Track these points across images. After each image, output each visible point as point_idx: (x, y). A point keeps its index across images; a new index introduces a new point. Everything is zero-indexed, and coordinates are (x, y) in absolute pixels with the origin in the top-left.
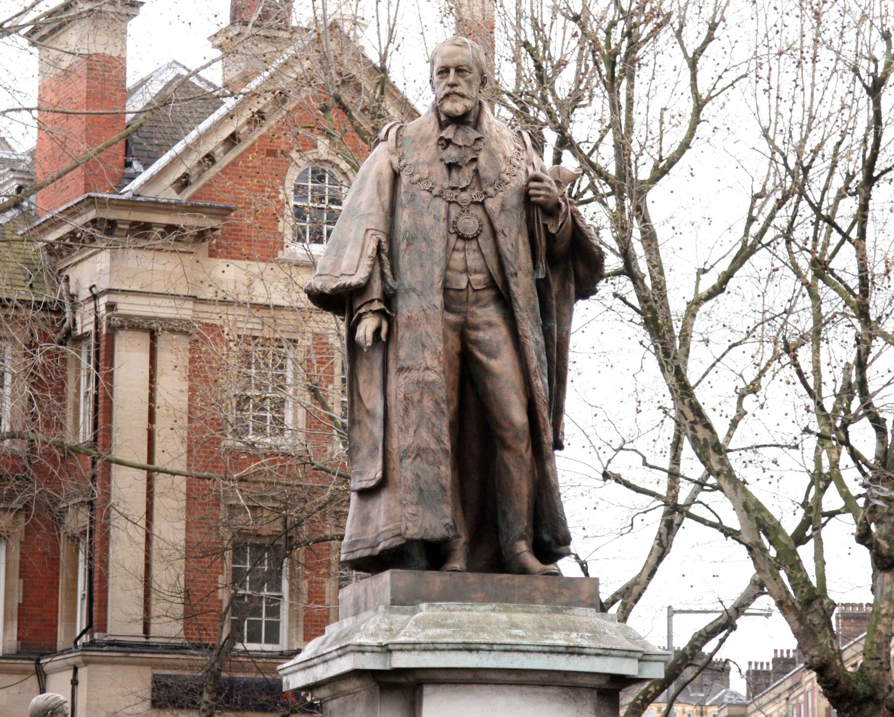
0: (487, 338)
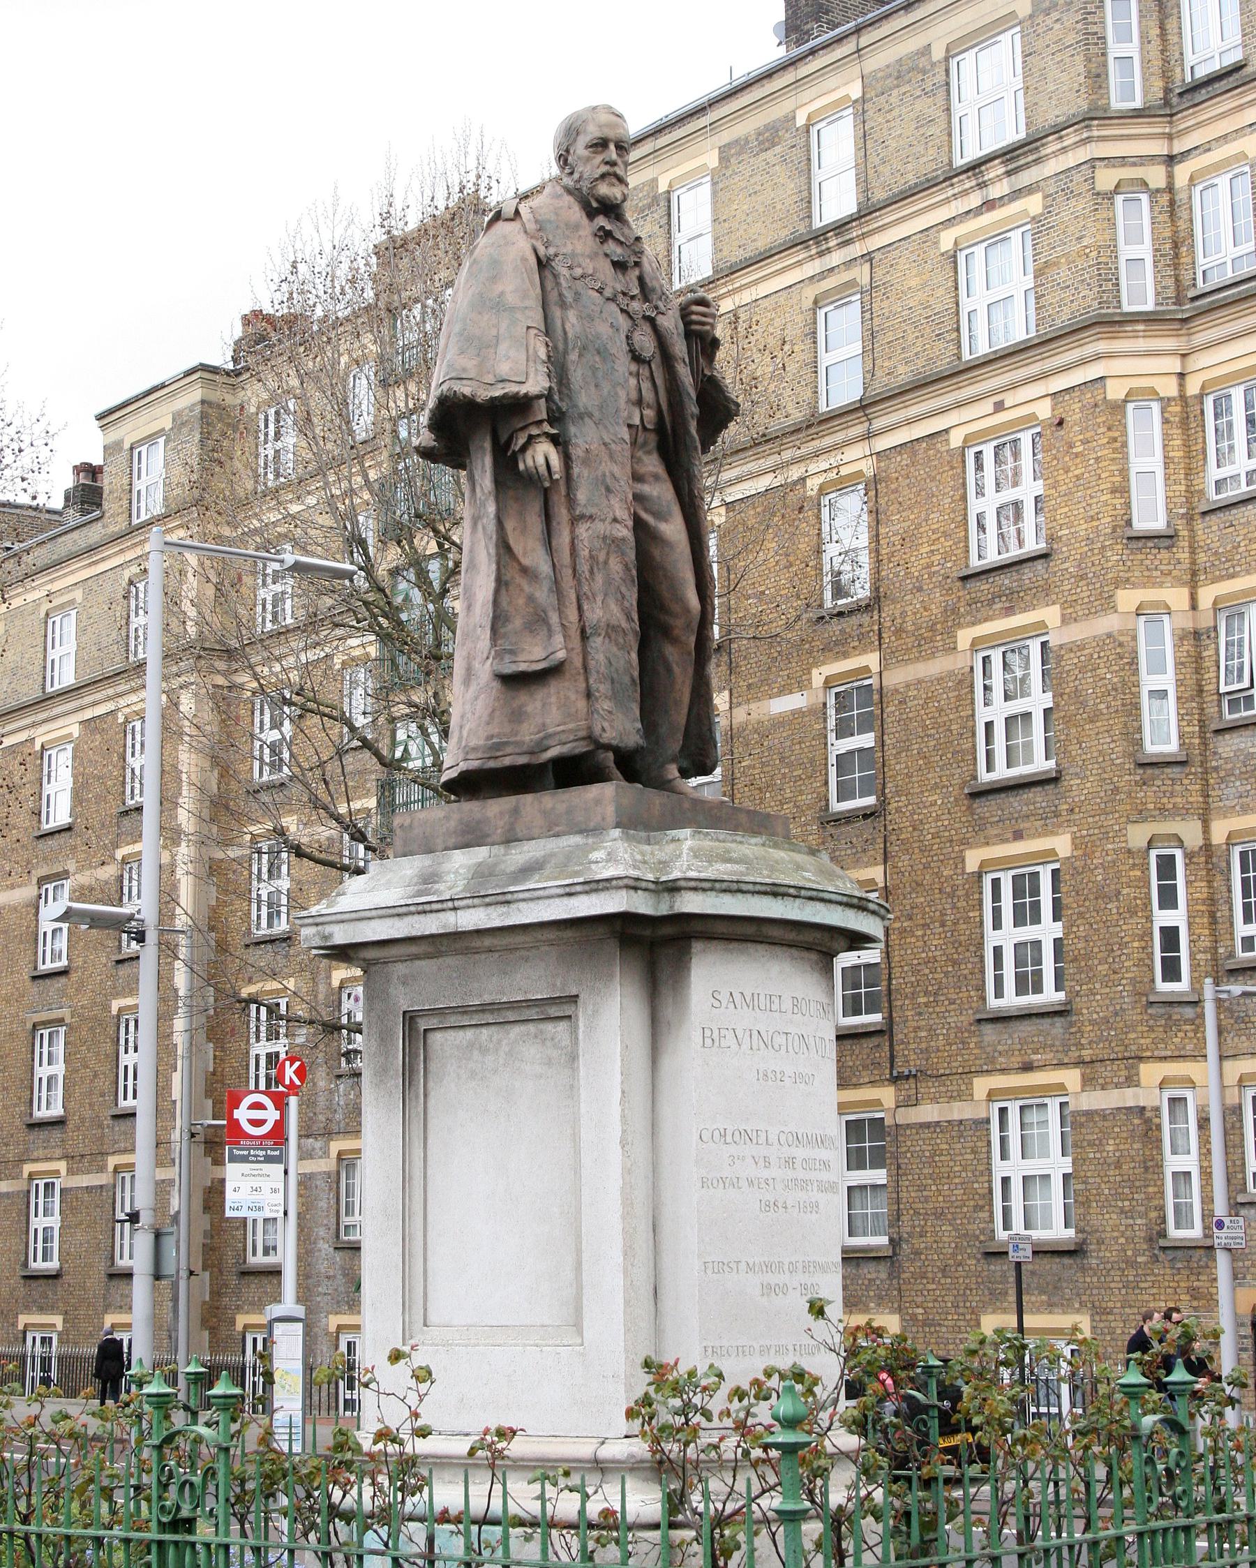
0: (655, 493)
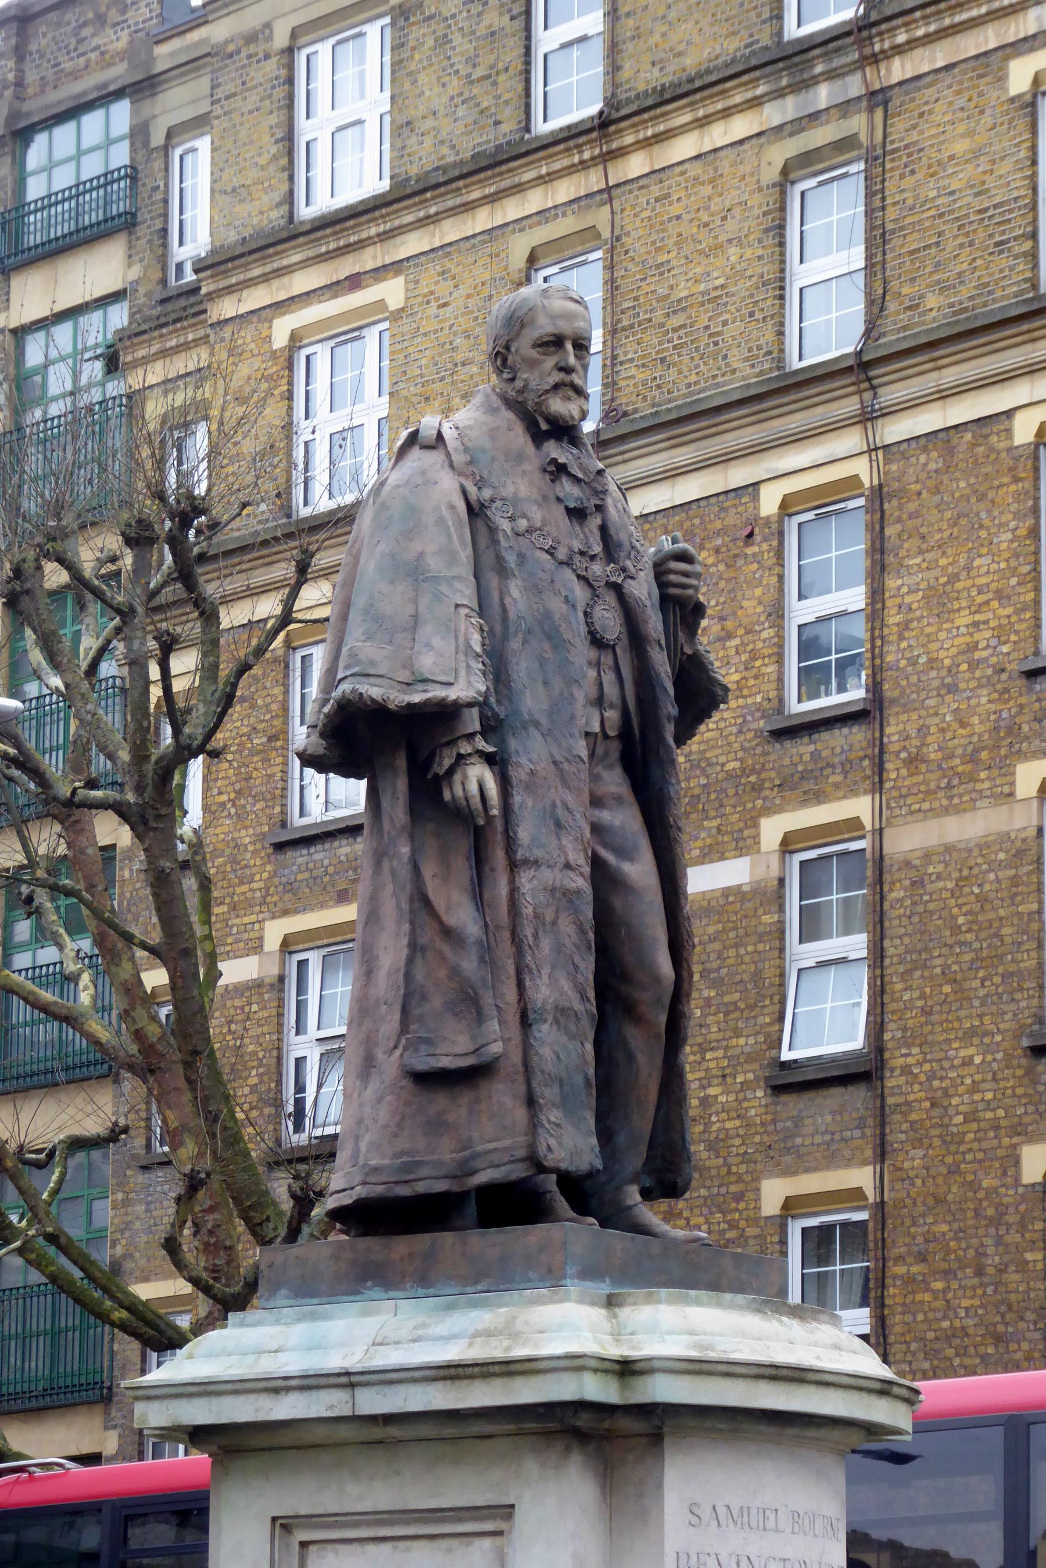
0: (617, 823)
